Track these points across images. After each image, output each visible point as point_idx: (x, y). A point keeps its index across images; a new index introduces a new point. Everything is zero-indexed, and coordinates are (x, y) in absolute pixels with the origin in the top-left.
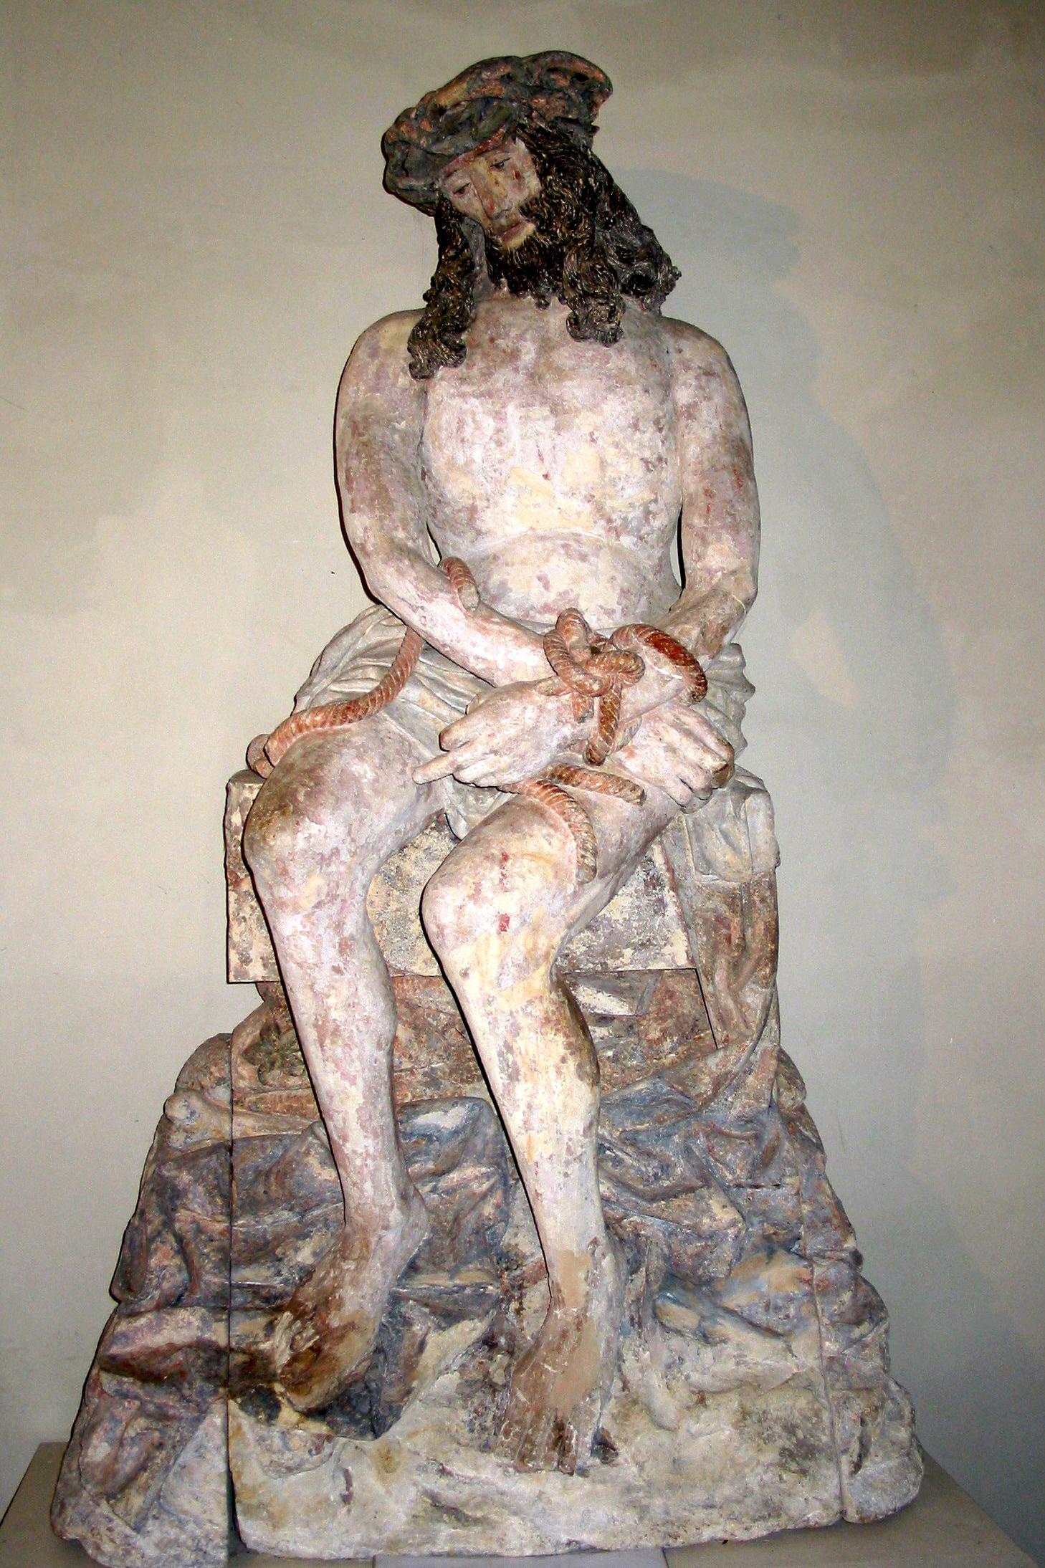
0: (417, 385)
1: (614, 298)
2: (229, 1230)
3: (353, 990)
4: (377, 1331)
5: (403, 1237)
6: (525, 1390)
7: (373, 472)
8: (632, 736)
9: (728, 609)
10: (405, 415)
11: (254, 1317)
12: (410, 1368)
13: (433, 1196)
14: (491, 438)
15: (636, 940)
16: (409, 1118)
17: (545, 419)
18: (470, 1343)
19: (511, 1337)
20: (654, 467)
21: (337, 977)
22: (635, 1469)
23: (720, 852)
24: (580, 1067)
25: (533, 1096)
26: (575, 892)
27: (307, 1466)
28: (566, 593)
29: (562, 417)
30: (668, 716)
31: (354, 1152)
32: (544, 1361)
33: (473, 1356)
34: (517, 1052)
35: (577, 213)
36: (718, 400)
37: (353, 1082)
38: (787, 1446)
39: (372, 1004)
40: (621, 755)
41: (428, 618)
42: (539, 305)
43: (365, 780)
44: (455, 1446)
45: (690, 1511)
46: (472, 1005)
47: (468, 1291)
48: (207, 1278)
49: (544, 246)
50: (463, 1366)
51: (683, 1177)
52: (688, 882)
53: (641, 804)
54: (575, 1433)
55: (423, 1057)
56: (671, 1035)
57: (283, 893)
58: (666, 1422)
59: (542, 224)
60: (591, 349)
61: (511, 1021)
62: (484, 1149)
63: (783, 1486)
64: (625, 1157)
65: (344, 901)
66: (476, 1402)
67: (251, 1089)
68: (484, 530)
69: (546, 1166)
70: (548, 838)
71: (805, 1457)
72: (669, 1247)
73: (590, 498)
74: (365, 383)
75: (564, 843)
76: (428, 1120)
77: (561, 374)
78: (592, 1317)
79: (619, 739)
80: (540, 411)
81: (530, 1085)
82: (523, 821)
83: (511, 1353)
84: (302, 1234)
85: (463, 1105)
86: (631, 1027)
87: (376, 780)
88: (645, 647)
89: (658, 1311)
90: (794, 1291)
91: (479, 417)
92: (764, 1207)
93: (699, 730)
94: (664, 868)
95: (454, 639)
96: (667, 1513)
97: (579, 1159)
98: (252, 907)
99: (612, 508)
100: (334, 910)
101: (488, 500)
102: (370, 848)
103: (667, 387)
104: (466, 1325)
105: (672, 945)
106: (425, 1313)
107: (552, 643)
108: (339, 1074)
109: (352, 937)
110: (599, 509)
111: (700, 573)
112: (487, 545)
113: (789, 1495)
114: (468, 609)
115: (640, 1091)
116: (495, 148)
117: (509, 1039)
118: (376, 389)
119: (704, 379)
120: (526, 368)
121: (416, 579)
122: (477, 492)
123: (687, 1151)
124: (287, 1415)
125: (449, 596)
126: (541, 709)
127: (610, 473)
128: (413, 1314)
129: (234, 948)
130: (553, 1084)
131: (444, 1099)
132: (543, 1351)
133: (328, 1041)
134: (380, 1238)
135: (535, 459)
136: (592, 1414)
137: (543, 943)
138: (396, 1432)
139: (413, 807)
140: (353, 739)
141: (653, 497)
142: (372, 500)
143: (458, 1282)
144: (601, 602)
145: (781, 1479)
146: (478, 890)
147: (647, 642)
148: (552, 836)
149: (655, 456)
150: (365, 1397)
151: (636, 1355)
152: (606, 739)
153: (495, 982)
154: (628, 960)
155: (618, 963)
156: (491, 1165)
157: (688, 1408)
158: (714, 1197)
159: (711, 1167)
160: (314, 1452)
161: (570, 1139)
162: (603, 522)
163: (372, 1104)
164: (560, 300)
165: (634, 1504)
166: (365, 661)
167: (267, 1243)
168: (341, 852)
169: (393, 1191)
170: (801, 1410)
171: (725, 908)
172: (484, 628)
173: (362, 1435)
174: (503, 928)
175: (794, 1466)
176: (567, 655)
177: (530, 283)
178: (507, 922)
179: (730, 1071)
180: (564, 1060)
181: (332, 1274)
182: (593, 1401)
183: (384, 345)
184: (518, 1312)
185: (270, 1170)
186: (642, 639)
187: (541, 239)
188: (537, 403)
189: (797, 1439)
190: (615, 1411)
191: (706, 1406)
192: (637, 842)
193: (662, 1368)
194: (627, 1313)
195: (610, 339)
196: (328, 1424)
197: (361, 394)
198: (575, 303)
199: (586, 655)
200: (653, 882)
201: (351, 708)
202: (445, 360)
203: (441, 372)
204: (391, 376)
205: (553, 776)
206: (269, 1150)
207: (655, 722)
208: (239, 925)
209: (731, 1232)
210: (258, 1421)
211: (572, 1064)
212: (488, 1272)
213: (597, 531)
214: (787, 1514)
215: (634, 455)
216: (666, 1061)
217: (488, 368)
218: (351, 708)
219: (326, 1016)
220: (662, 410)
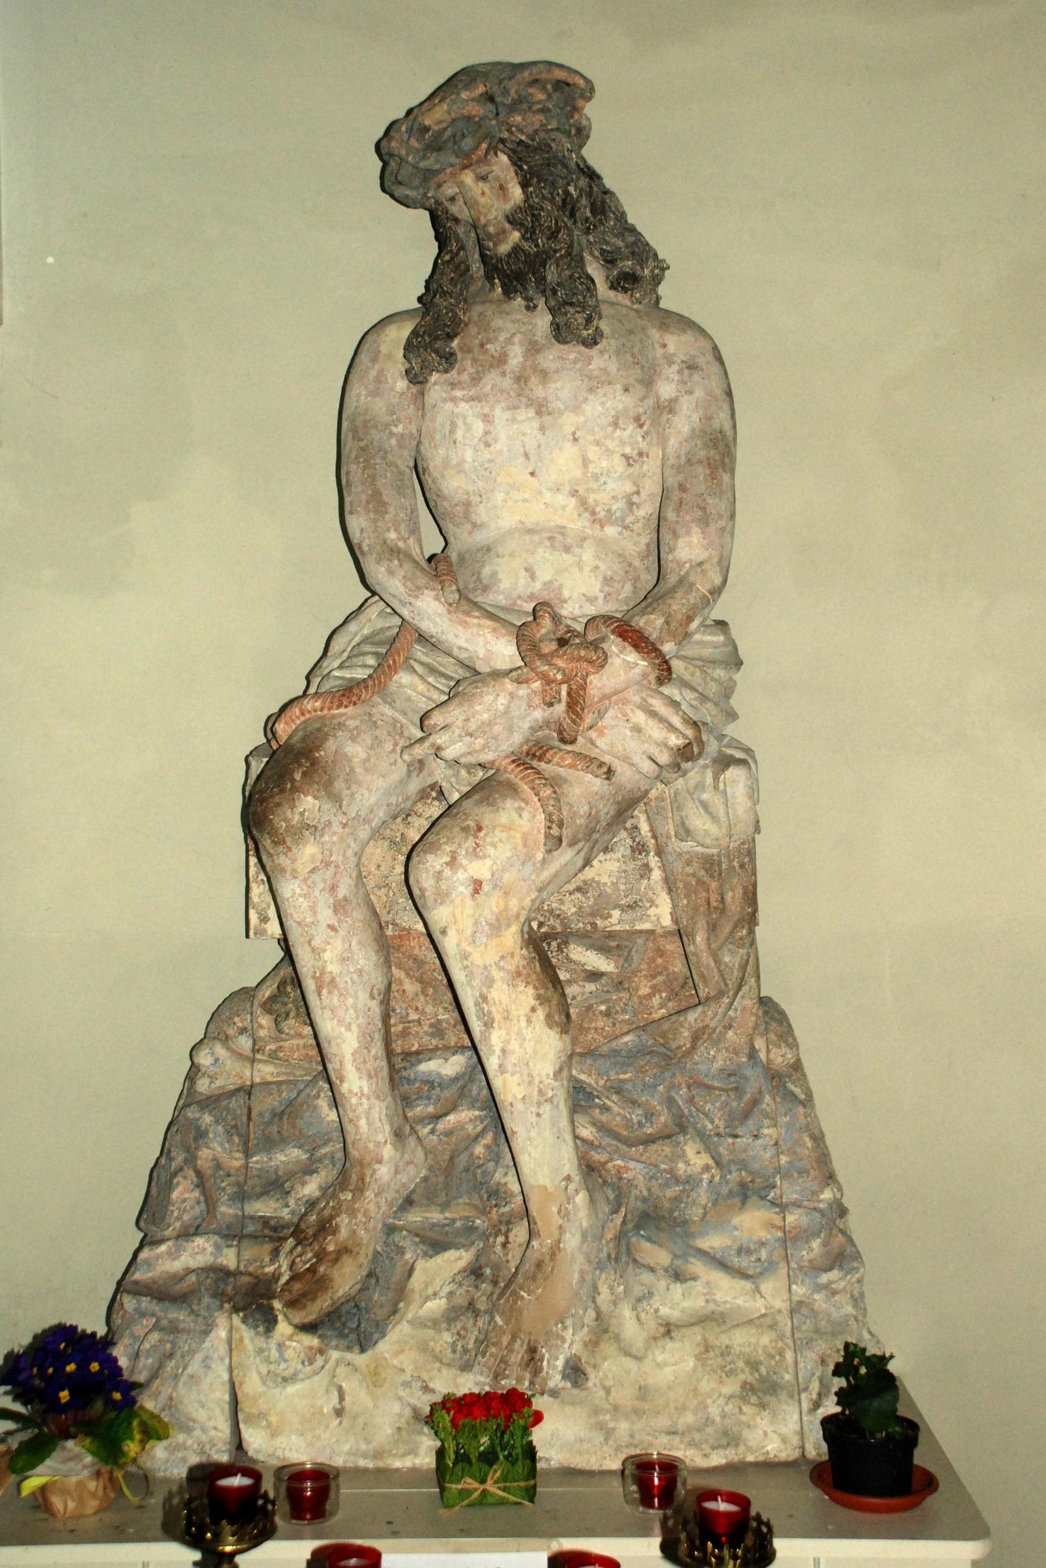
0: (414, 389)
2: (246, 1166)
3: (347, 945)
4: (370, 1257)
5: (397, 1172)
6: (502, 1314)
7: (369, 477)
8: (601, 718)
9: (692, 598)
11: (262, 1244)
12: (401, 1293)
13: (431, 1137)
14: (480, 440)
15: (623, 902)
16: (413, 1065)
17: (529, 419)
18: (456, 1271)
19: (497, 1268)
21: (332, 934)
22: (602, 1393)
23: (699, 822)
24: (549, 1016)
25: (507, 1042)
26: (544, 859)
27: (301, 1376)
28: (551, 582)
29: (547, 419)
31: (350, 1092)
32: (521, 1289)
33: (461, 1285)
34: (492, 1002)
36: (699, 393)
37: (348, 1028)
38: (749, 1381)
39: (366, 958)
40: (593, 734)
42: (528, 308)
43: (357, 760)
44: (438, 1364)
45: (653, 1436)
47: (458, 1224)
48: (223, 1209)
50: (451, 1294)
51: (666, 1125)
52: (670, 848)
53: (608, 779)
54: (547, 1356)
55: (429, 1009)
56: (660, 991)
57: (283, 860)
58: (634, 1351)
59: (526, 232)
60: (573, 352)
61: (486, 973)
62: (479, 1094)
63: (743, 1418)
64: (612, 1105)
65: (337, 867)
66: (459, 1325)
67: (270, 1037)
68: (478, 523)
69: (519, 1106)
70: (519, 811)
71: (766, 1392)
72: (649, 1190)
73: (574, 493)
74: (366, 388)
75: (534, 816)
76: (429, 1067)
77: (544, 376)
78: (565, 1249)
79: (588, 719)
80: (527, 414)
81: (503, 1032)
82: (497, 796)
83: (495, 1283)
84: (308, 1170)
85: (462, 1053)
86: (621, 983)
87: (368, 759)
88: (612, 637)
89: (632, 1248)
90: (763, 1234)
91: (469, 420)
92: (743, 1156)
94: (649, 834)
96: (632, 1436)
97: (550, 1100)
99: (596, 501)
100: (328, 874)
102: (361, 820)
103: (648, 383)
104: (451, 1254)
105: (657, 906)
106: (416, 1243)
107: (522, 636)
108: (335, 1021)
109: (345, 899)
110: (583, 503)
111: (670, 565)
112: (480, 537)
113: (749, 1427)
114: (450, 605)
115: (626, 1043)
117: (484, 990)
119: (686, 372)
120: (513, 372)
121: (404, 577)
122: (470, 488)
123: (670, 1102)
124: (283, 1328)
125: (433, 593)
126: (512, 695)
127: (592, 468)
128: (407, 1243)
130: (524, 1031)
131: (446, 1048)
132: (520, 1279)
133: (325, 992)
134: (374, 1171)
135: (521, 460)
136: (564, 1340)
137: (514, 905)
138: (384, 1347)
139: (403, 783)
140: (348, 723)
141: (634, 489)
142: (368, 502)
143: (447, 1215)
144: (583, 590)
145: (740, 1409)
147: (613, 632)
148: (523, 809)
149: (636, 452)
150: (355, 1314)
151: (611, 1288)
152: (574, 721)
153: (471, 940)
154: (615, 921)
155: (607, 923)
156: (482, 1109)
157: (655, 1339)
158: (690, 1143)
159: (692, 1116)
160: (306, 1363)
161: (541, 1082)
162: (587, 514)
163: (366, 1048)
165: (601, 1426)
166: (368, 648)
167: (278, 1178)
168: (334, 825)
169: (387, 1128)
170: (765, 1347)
171: (703, 872)
172: (466, 622)
173: (349, 1348)
175: (753, 1399)
176: (535, 647)
177: (519, 287)
178: (480, 886)
179: (707, 1026)
180: (533, 1010)
181: (331, 1204)
182: (565, 1328)
184: (504, 1245)
185: (283, 1111)
186: (609, 629)
187: (526, 245)
188: (523, 406)
189: (760, 1375)
190: (587, 1339)
191: (671, 1338)
192: (607, 814)
193: (633, 1300)
194: (605, 1249)
195: (591, 342)
196: (320, 1337)
197: (362, 398)
199: (554, 646)
200: (639, 848)
201: (349, 692)
203: (435, 377)
204: (390, 380)
205: (528, 754)
206: (284, 1094)
209: (706, 1177)
210: (257, 1333)
211: (541, 1014)
212: (476, 1207)
213: (577, 524)
214: (745, 1444)
216: (656, 1016)
218: (349, 692)
219: (324, 968)
220: (643, 407)
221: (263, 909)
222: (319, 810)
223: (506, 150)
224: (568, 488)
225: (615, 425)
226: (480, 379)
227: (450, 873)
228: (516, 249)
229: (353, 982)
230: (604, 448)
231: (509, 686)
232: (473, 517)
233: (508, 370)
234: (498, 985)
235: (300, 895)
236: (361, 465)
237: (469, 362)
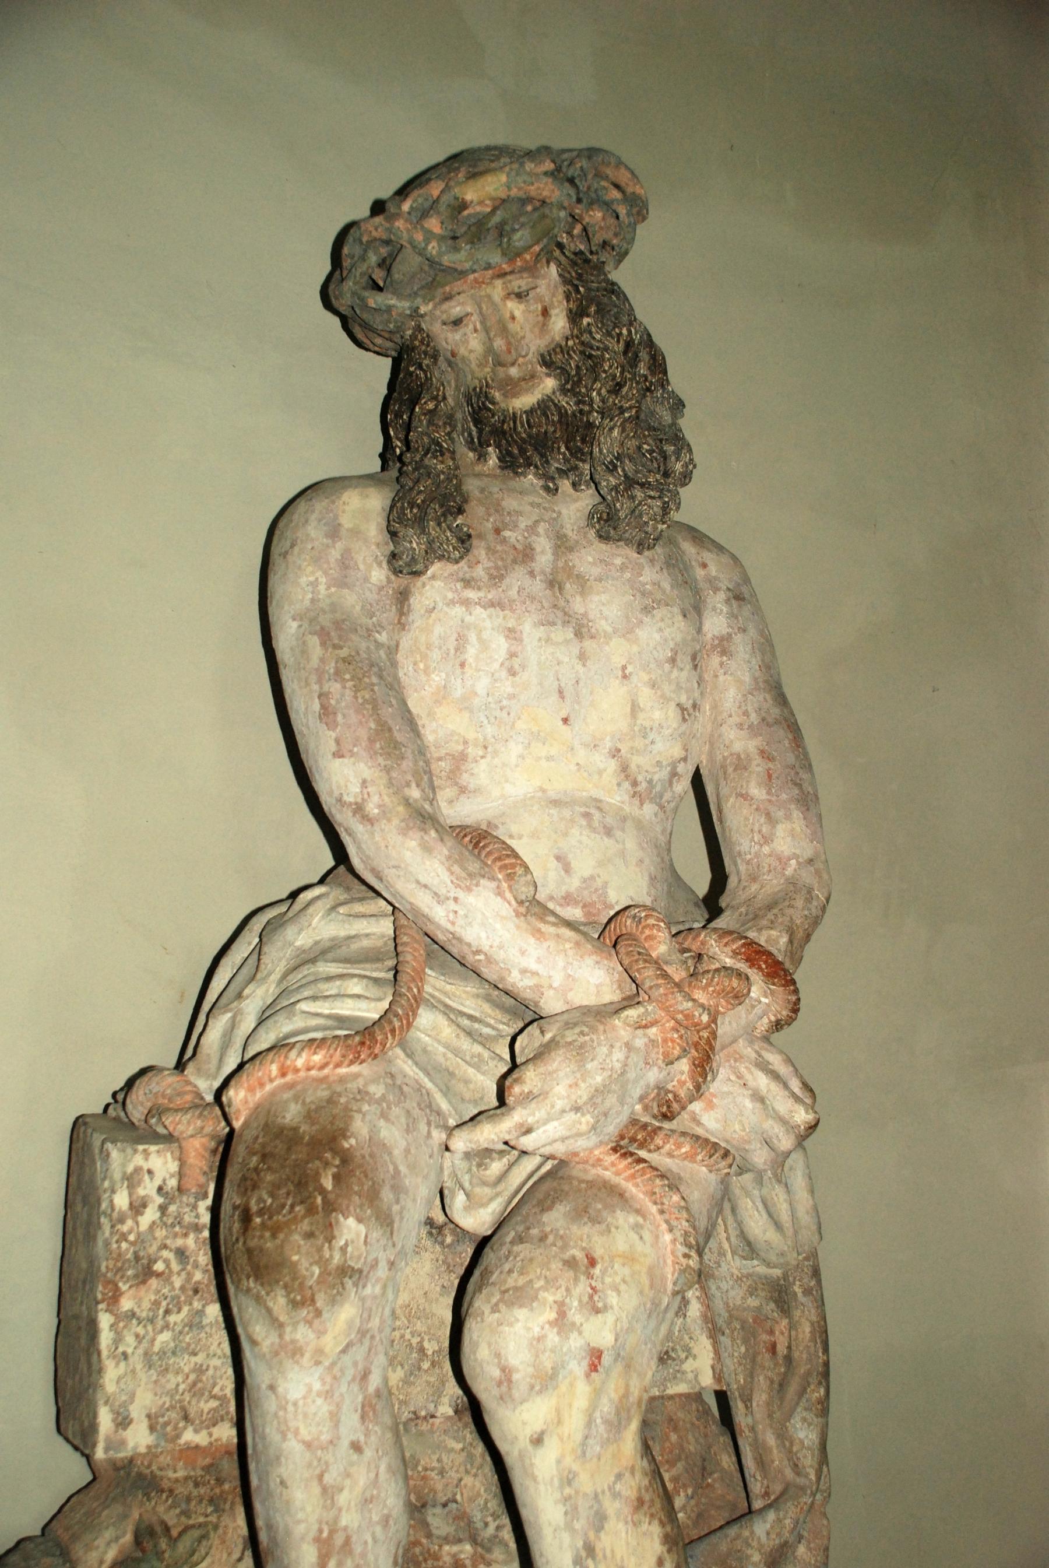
1: (669, 491)
3: (372, 1475)
10: (385, 623)
14: (502, 664)
17: (567, 642)
20: (689, 715)
21: (355, 1457)
28: (592, 878)
29: (588, 644)
30: (749, 1052)
34: (600, 1555)
35: (622, 373)
41: (461, 913)
42: (547, 489)
46: (542, 1488)
49: (566, 411)
56: (685, 1486)
59: (567, 382)
60: (622, 555)
68: (471, 787)
73: (615, 753)
74: (326, 573)
77: (583, 584)
80: (563, 634)
91: (486, 635)
93: (784, 1070)
95: (495, 944)
98: (137, 1336)
99: (638, 767)
101: (486, 747)
105: (695, 1357)
110: (624, 768)
114: (521, 903)
116: (523, 270)
117: (592, 1535)
118: (342, 583)
120: (543, 572)
122: (471, 735)
125: (494, 885)
126: (628, 1046)
129: (106, 1403)
135: (555, 697)
141: (683, 754)
146: (562, 1314)
148: (642, 1227)
162: (626, 785)
164: (575, 485)
172: (539, 931)
174: (594, 1368)
177: (537, 459)
178: (599, 1357)
183: (347, 522)
186: (728, 949)
188: (559, 622)
197: (322, 588)
198: (617, 492)
202: (449, 553)
203: (436, 568)
204: (361, 567)
207: (736, 1061)
208: (117, 1364)
215: (669, 700)
217: (497, 568)
219: (336, 1520)
221: (124, 1405)
222: (365, 1242)
223: (562, 259)
224: (608, 745)
225: (673, 660)
226: (502, 577)
227: (557, 1339)
228: (544, 406)
229: (375, 1541)
230: (659, 693)
231: (622, 1033)
232: (465, 778)
233: (537, 570)
234: (611, 1524)
235: (319, 1395)
236: (350, 684)
237: (483, 552)
